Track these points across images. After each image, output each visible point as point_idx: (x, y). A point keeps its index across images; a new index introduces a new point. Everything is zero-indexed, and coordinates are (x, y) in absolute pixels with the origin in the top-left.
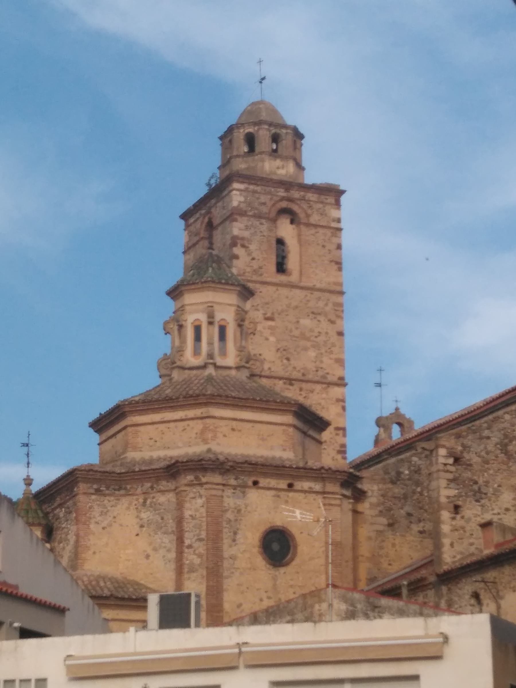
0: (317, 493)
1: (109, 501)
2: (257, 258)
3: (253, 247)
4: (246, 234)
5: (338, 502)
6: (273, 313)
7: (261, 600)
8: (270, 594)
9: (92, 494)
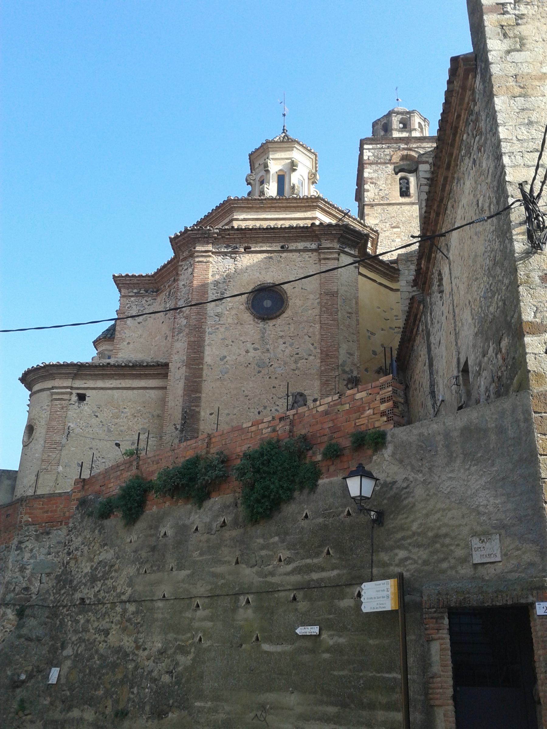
0: (312, 250)
1: (147, 301)
3: (381, 183)
4: (374, 175)
5: (336, 256)
6: (398, 223)
7: (247, 352)
8: (256, 346)
9: (132, 296)
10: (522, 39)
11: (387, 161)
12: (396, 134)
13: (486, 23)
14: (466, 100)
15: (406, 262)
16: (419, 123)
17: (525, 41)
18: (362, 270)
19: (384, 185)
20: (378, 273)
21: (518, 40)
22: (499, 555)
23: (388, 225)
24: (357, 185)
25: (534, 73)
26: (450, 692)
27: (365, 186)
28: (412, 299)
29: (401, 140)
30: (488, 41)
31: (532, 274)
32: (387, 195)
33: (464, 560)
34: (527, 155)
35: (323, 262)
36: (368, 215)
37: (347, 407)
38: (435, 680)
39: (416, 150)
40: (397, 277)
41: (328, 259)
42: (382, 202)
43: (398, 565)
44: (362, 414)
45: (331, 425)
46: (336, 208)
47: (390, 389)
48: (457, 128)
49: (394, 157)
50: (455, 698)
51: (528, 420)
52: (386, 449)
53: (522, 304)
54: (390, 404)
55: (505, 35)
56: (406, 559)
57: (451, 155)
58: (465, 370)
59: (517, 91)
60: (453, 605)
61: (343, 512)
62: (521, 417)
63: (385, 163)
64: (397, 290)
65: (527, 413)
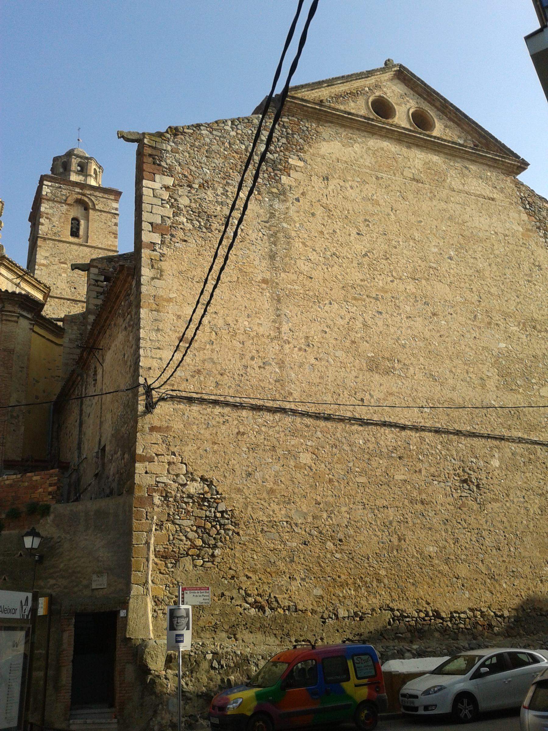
2: (56, 226)
4: (50, 211)
5: (15, 319)
10: (162, 271)
11: (63, 201)
12: (74, 178)
13: (143, 255)
14: (126, 287)
15: (71, 322)
16: (95, 169)
17: (163, 273)
18: (36, 329)
19: (57, 223)
20: (47, 330)
21: (159, 271)
22: (106, 585)
23: (57, 259)
24: (32, 209)
25: (165, 297)
26: (71, 658)
27: (41, 219)
28: (73, 371)
29: (76, 184)
30: (142, 268)
31: (145, 426)
32: (59, 232)
33: (87, 586)
34: (153, 350)
35: (4, 322)
36: (40, 247)
37: (26, 484)
38: (64, 653)
39: (89, 196)
40: (62, 335)
41: (9, 321)
42: (53, 238)
43: (49, 588)
44: (36, 490)
45: (13, 494)
46: (17, 267)
47: (56, 478)
48: (118, 297)
49: (69, 198)
50: (73, 661)
51: (131, 511)
52: (49, 516)
53: (137, 443)
54: (55, 487)
55: (152, 266)
56: (54, 585)
57: (113, 307)
58: (103, 449)
59: (154, 306)
60: (78, 611)
61: (17, 553)
62: (127, 509)
63: (61, 203)
64: (61, 345)
65: (131, 507)
